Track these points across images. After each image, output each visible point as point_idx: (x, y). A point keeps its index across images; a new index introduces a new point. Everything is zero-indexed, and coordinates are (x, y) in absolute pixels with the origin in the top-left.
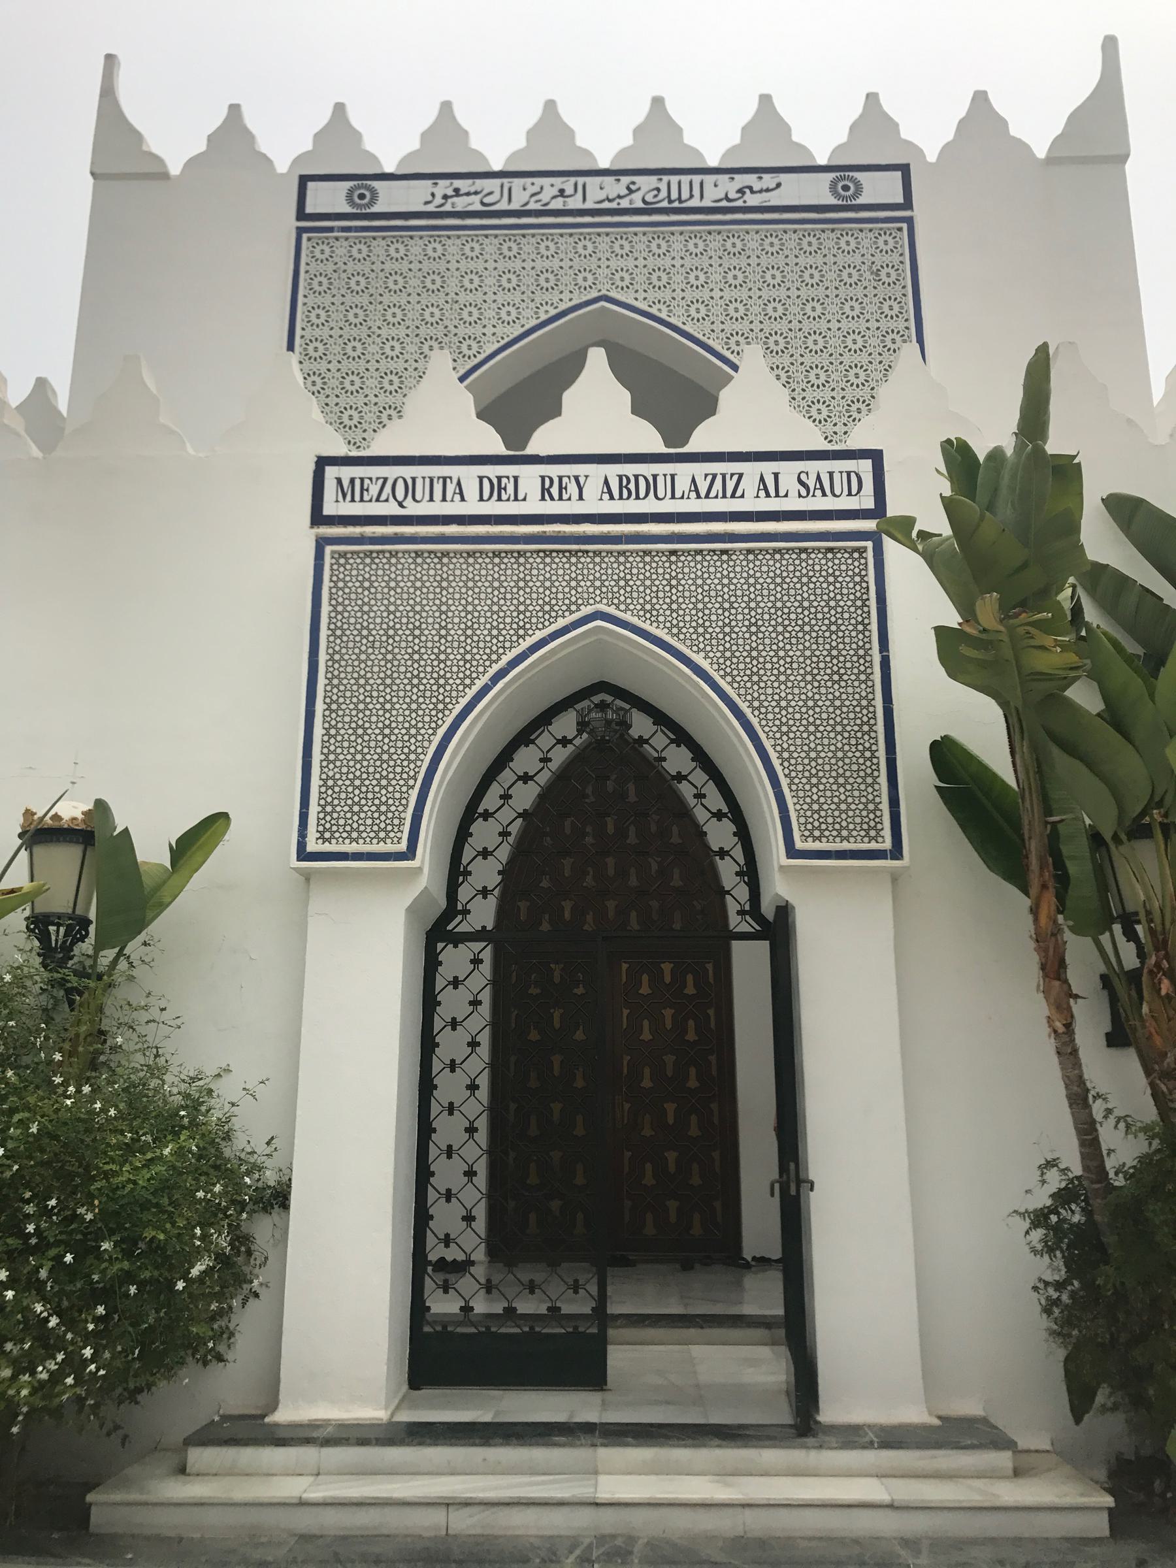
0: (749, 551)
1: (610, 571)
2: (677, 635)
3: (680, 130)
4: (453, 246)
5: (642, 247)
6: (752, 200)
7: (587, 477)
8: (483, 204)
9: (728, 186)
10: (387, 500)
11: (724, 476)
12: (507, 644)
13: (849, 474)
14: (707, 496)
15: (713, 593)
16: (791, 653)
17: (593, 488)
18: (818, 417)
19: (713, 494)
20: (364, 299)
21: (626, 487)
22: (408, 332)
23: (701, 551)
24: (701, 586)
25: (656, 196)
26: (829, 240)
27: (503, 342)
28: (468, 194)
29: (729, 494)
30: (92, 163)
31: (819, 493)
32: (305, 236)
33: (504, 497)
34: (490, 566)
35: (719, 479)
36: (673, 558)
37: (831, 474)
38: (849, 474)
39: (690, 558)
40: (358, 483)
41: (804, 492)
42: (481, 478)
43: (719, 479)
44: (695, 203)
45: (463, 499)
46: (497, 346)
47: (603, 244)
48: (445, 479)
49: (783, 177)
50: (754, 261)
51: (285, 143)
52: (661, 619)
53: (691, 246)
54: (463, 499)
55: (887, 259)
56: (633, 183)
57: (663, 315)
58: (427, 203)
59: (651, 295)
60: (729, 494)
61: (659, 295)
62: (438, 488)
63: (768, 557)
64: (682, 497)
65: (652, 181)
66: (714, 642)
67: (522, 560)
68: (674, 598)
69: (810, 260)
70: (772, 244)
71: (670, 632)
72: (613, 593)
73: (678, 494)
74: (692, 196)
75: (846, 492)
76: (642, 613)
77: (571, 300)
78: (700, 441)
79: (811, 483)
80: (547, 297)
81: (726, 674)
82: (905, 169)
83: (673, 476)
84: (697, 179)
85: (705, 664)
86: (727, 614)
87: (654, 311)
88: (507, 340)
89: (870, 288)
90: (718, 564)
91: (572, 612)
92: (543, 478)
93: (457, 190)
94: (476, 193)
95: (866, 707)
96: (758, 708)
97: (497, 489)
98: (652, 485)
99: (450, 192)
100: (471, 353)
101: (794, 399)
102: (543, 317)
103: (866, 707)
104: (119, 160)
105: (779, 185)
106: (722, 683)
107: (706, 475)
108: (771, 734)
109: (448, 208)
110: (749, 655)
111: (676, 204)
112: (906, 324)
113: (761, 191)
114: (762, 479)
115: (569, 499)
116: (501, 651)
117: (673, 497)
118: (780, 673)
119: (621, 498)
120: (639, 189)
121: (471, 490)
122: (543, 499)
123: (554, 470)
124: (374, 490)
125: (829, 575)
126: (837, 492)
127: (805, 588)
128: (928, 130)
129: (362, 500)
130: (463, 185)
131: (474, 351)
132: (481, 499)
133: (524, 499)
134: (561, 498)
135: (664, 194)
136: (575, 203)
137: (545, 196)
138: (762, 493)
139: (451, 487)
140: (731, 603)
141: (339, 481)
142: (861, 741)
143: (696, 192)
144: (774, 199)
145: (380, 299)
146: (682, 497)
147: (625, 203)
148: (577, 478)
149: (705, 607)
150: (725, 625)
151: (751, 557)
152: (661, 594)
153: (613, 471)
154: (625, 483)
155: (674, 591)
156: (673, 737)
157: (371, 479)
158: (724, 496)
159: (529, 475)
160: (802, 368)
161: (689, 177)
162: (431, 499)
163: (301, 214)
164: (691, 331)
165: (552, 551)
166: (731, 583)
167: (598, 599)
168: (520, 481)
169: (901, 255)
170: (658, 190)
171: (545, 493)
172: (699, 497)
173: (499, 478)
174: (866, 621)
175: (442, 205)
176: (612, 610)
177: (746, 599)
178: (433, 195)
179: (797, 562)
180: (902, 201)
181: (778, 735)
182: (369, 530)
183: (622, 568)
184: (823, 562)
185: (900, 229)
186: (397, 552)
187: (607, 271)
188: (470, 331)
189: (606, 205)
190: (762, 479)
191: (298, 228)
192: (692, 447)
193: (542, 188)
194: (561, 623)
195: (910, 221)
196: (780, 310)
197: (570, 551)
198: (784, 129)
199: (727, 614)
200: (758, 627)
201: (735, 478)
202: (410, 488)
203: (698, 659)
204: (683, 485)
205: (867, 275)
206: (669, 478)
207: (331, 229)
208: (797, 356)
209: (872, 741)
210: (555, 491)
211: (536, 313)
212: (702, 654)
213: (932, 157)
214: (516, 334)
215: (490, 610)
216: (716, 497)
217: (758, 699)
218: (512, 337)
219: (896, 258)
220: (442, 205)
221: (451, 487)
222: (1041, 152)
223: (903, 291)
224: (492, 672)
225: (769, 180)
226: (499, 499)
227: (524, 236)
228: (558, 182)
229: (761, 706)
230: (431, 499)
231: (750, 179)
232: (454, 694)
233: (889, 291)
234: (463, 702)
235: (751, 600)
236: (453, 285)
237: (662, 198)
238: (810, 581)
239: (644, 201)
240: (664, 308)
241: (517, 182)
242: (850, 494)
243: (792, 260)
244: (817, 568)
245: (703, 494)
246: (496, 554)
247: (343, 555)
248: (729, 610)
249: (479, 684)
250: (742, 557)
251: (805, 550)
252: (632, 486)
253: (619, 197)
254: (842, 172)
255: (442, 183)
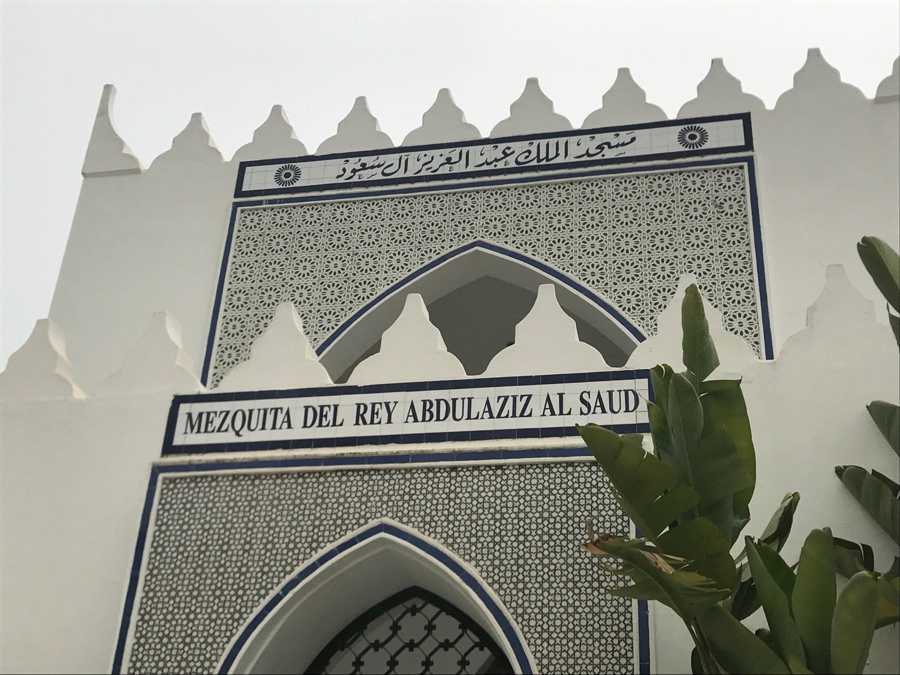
0: (521, 466)
1: (397, 487)
2: (452, 545)
3: (550, 103)
4: (357, 209)
5: (678, 184)
6: (609, 154)
7: (396, 403)
8: (383, 174)
9: (589, 144)
10: (226, 430)
11: (515, 397)
12: (301, 557)
13: (626, 392)
14: (499, 416)
15: (486, 505)
16: (555, 561)
17: (400, 413)
18: (740, 329)
19: (504, 414)
20: (282, 257)
21: (429, 410)
22: (315, 281)
23: (479, 466)
24: (477, 499)
25: (527, 157)
26: (677, 182)
27: (392, 285)
28: (372, 167)
29: (518, 413)
30: (84, 166)
31: (599, 410)
32: (239, 209)
33: (324, 423)
34: (540, 476)
35: (510, 400)
36: (453, 474)
37: (610, 393)
38: (626, 392)
39: (468, 473)
40: (204, 417)
41: (585, 410)
42: (307, 408)
43: (510, 400)
44: (560, 160)
45: (289, 427)
46: (387, 288)
47: (481, 199)
48: (276, 410)
49: (636, 133)
50: (609, 204)
51: (231, 139)
52: (439, 530)
53: (555, 195)
54: (289, 427)
55: (729, 193)
56: (509, 148)
57: (529, 255)
58: (338, 177)
59: (519, 239)
60: (518, 413)
61: (526, 238)
62: (270, 418)
63: (538, 470)
64: (477, 418)
65: (525, 145)
66: (485, 551)
67: (322, 480)
68: (452, 510)
69: (660, 200)
70: (626, 189)
71: (445, 542)
72: (398, 506)
73: (473, 415)
74: (557, 155)
75: (623, 408)
76: (422, 525)
77: (451, 247)
78: (494, 370)
79: (592, 401)
80: (431, 245)
81: (494, 582)
82: (746, 118)
83: (470, 399)
84: (562, 141)
85: (474, 572)
86: (522, 523)
87: (521, 251)
88: (395, 282)
89: (714, 219)
90: (493, 478)
91: (360, 525)
92: (359, 405)
93: (364, 166)
94: (379, 166)
95: (624, 614)
96: (522, 615)
97: (320, 416)
98: (451, 409)
99: (358, 167)
100: (365, 295)
101: (643, 319)
102: (427, 262)
103: (624, 614)
104: (107, 163)
105: (633, 140)
106: (489, 591)
107: (499, 398)
108: (532, 641)
109: (355, 179)
110: (516, 563)
111: (544, 162)
112: (747, 248)
113: (617, 146)
114: (548, 399)
115: (380, 423)
116: (295, 563)
117: (469, 418)
118: (544, 580)
119: (424, 420)
120: (513, 152)
121: (297, 419)
122: (357, 423)
123: (368, 399)
124: (217, 422)
125: (592, 486)
126: (616, 409)
127: (570, 499)
128: (766, 83)
129: (206, 431)
130: (369, 160)
131: (367, 294)
132: (305, 426)
133: (569, 413)
134: (372, 423)
135: (534, 155)
136: (459, 168)
137: (435, 165)
138: (548, 412)
139: (281, 417)
140: (502, 514)
141: (190, 416)
142: (618, 648)
143: (562, 151)
144: (629, 151)
145: (294, 255)
146: (477, 418)
147: (501, 165)
148: (387, 404)
149: (479, 518)
150: (495, 535)
151: (522, 471)
152: (440, 507)
153: (418, 397)
154: (428, 407)
155: (452, 503)
156: (477, 640)
157: (216, 413)
158: (514, 416)
159: (347, 404)
160: (651, 292)
161: (556, 140)
162: (263, 428)
163: (239, 192)
164: (552, 266)
165: (348, 471)
166: (503, 495)
167: (384, 512)
168: (339, 409)
169: (742, 189)
170: (529, 152)
171: (360, 418)
172: (491, 417)
173: (322, 407)
174: (626, 530)
175: (351, 177)
176: (395, 523)
177: (516, 510)
178: (344, 170)
179: (564, 475)
180: (743, 144)
181: (539, 642)
182: (196, 458)
183: (546, 478)
184: (516, 477)
185: (742, 167)
186: (217, 477)
187: (483, 221)
188: (365, 277)
189: (485, 167)
190: (548, 399)
191: (234, 203)
192: (488, 374)
193: (432, 158)
194: (350, 535)
195: (750, 161)
196: (632, 243)
197: (364, 470)
198: (735, 83)
199: (498, 524)
200: (526, 537)
201: (525, 398)
202: (247, 420)
203: (469, 567)
204: (478, 407)
205: (712, 208)
206: (466, 401)
207: (260, 203)
208: (646, 282)
209: (627, 648)
210: (368, 416)
211: (421, 259)
212: (474, 563)
213: (770, 104)
214: (403, 277)
215: (470, 519)
216: (507, 416)
217: (522, 606)
218: (400, 280)
219: (738, 192)
220: (351, 177)
221: (281, 417)
222: (870, 94)
223: (745, 220)
224: (284, 582)
225: (624, 136)
226: (320, 425)
227: (324, 205)
228: (446, 152)
229: (525, 612)
230: (263, 428)
231: (609, 137)
232: (250, 604)
233: (732, 221)
234: (257, 611)
235: (520, 511)
236: (354, 240)
237: (538, 159)
238: (575, 492)
239: (517, 162)
240: (530, 248)
241: (413, 155)
242: (627, 410)
243: (643, 201)
244: (582, 480)
245: (495, 414)
246: (301, 475)
247: (173, 481)
248: (500, 520)
249: (272, 594)
250: (514, 471)
251: (571, 464)
252: (434, 410)
253: (496, 160)
254: (690, 125)
255: (352, 160)
